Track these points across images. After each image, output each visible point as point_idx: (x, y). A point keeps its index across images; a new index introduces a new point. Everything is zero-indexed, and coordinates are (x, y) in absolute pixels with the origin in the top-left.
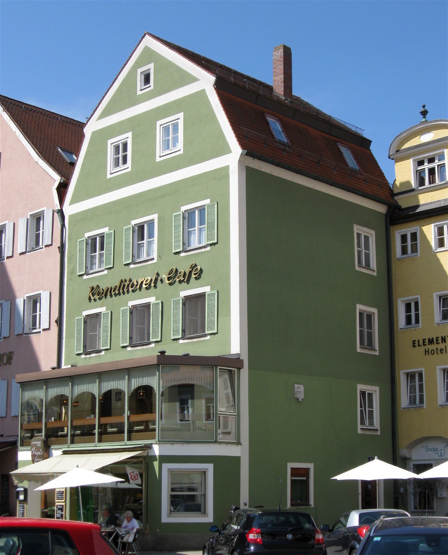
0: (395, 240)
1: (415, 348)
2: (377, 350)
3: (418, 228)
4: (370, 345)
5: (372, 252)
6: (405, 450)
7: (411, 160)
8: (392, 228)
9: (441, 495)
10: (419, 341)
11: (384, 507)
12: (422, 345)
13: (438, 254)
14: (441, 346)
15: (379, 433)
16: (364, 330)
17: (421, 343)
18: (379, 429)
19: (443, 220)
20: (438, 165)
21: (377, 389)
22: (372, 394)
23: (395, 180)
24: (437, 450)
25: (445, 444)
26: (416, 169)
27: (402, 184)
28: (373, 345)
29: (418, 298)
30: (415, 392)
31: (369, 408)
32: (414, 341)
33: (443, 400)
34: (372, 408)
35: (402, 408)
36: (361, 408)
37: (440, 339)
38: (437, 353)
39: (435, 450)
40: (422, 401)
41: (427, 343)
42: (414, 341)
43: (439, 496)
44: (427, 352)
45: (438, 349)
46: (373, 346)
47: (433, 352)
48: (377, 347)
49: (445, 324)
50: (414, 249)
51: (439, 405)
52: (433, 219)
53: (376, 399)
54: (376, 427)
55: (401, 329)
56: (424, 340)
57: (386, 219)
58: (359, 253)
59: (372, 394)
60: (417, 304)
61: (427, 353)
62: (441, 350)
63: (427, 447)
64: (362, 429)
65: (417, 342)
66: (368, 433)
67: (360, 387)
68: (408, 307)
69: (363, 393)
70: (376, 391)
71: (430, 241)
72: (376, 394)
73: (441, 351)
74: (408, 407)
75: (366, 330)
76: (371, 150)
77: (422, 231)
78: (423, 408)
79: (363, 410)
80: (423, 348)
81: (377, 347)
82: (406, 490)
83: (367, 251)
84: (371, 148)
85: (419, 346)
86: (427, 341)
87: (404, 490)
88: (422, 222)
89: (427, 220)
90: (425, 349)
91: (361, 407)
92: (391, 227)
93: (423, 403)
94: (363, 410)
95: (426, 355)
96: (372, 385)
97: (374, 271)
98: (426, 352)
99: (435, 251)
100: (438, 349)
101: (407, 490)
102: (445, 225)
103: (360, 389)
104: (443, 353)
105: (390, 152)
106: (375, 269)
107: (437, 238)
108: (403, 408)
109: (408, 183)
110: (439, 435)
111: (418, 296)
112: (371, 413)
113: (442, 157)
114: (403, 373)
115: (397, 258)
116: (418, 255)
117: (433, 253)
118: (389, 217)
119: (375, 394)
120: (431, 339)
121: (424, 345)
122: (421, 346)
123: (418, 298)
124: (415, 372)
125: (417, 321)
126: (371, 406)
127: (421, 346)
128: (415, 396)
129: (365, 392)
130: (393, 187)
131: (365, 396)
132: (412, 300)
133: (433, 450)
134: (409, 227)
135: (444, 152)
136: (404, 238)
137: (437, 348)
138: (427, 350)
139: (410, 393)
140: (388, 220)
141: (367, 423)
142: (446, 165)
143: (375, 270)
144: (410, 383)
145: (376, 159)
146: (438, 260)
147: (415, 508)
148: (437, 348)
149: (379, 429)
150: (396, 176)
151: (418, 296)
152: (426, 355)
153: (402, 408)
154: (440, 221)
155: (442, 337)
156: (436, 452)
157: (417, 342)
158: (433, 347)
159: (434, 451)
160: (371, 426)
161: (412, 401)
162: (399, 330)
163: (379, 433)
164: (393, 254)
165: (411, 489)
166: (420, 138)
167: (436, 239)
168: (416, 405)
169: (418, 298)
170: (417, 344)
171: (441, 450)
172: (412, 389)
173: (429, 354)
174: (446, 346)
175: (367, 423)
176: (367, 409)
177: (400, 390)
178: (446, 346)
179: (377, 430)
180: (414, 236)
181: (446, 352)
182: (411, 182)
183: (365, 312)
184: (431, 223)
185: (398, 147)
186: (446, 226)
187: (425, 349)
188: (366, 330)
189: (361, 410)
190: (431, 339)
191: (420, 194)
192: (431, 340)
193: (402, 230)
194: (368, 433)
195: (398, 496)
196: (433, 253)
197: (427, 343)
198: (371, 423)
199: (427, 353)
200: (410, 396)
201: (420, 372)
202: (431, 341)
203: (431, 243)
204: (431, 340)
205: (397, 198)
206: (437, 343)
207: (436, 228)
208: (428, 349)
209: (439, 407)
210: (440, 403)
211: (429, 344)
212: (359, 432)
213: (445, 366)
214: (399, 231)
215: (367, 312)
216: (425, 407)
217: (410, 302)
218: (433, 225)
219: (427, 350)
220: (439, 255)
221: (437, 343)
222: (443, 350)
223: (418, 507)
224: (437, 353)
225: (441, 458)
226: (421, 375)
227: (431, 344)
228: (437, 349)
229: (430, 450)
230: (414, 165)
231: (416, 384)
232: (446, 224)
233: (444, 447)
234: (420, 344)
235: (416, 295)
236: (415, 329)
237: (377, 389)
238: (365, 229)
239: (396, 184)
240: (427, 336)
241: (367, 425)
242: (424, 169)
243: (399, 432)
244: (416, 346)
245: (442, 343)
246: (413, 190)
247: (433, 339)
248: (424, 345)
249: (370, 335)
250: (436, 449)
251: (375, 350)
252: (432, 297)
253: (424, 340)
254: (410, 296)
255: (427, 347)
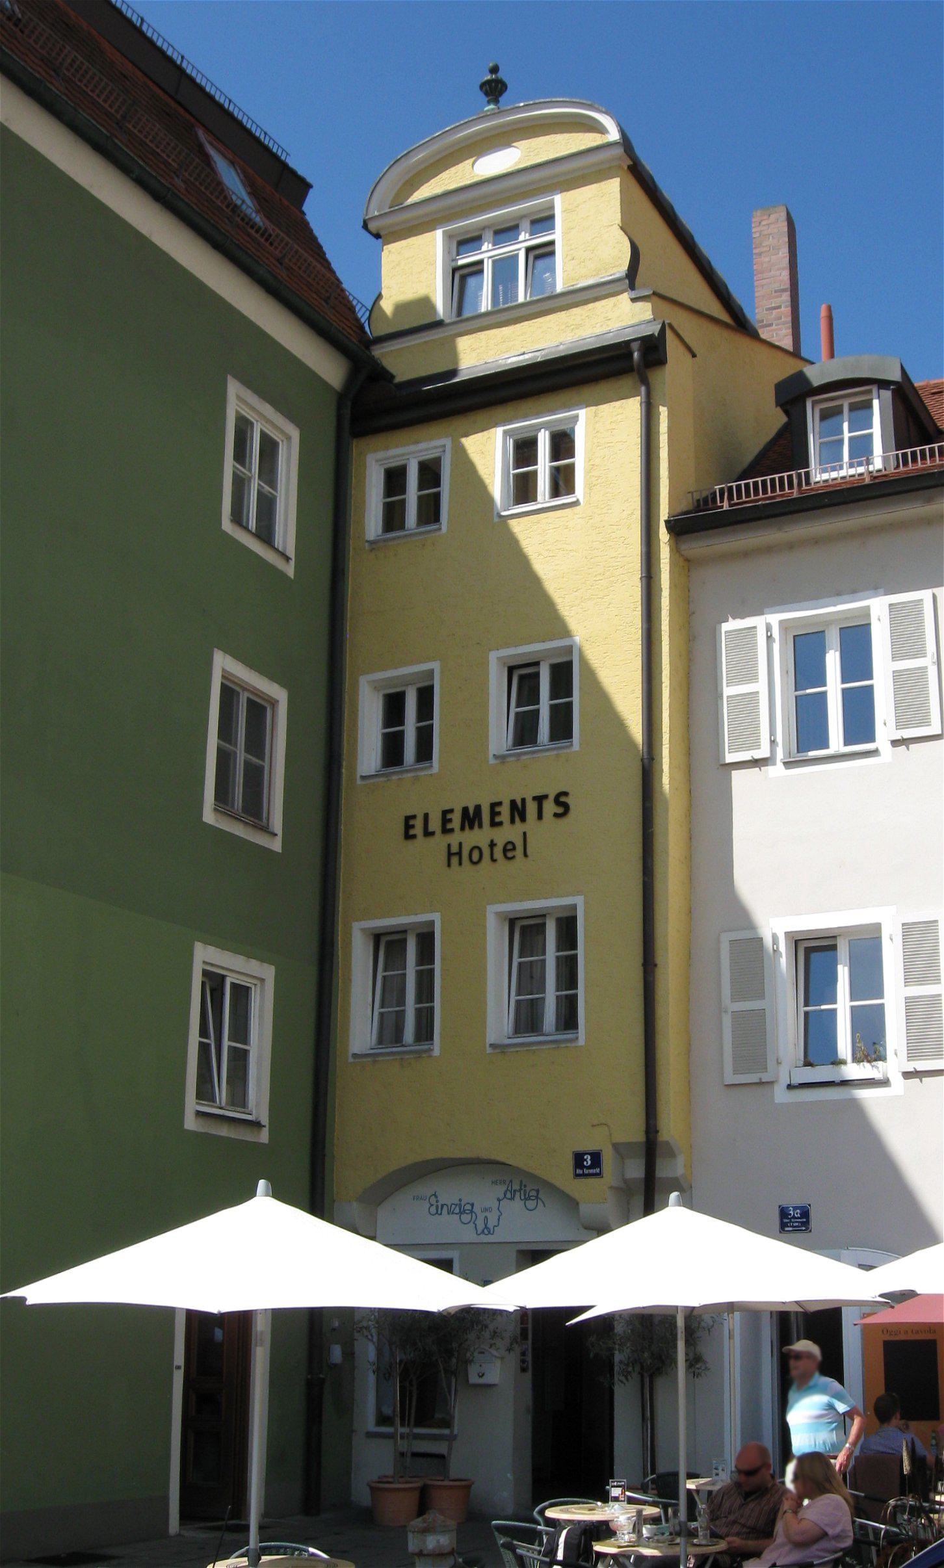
0: (365, 482)
1: (409, 843)
2: (276, 835)
3: (447, 442)
4: (254, 811)
5: (283, 492)
6: (355, 1204)
7: (439, 234)
8: (357, 447)
9: (481, 1376)
10: (426, 816)
11: (175, 1311)
12: (438, 831)
13: (513, 523)
14: (509, 832)
15: (264, 1137)
16: (235, 753)
17: (435, 824)
18: (265, 1121)
19: (538, 415)
20: (529, 250)
21: (268, 972)
22: (248, 989)
23: (379, 297)
24: (472, 1211)
25: (500, 1190)
26: (454, 264)
27: (401, 308)
28: (265, 815)
29: (431, 673)
30: (401, 1001)
31: (234, 1041)
32: (408, 819)
33: (506, 1028)
34: (245, 1041)
35: (350, 1055)
36: (201, 1036)
37: (505, 810)
38: (493, 860)
39: (463, 1210)
40: (425, 1031)
41: (456, 823)
42: (408, 819)
43: (474, 1379)
44: (453, 855)
45: (495, 845)
46: (265, 820)
47: (476, 856)
48: (277, 822)
49: (525, 757)
50: (430, 511)
51: (491, 1045)
52: (499, 412)
53: (261, 1010)
54: (254, 1112)
55: (363, 778)
56: (445, 813)
57: (340, 407)
58: (240, 484)
59: (248, 989)
60: (426, 696)
61: (455, 860)
62: (509, 848)
63: (433, 1200)
64: (199, 1114)
65: (419, 823)
66: (224, 1131)
67: (205, 955)
68: (394, 707)
69: (214, 982)
70: (262, 980)
71: (487, 481)
72: (289, 448)
73: (505, 850)
74: (372, 1051)
75: (241, 756)
76: (305, 211)
77: (461, 454)
78: (431, 1056)
79: (209, 1045)
80: (439, 842)
81: (277, 822)
82: (349, 1354)
83: (257, 761)
84: (305, 208)
85: (428, 833)
86: (456, 818)
87: (343, 1353)
88: (460, 422)
89: (480, 417)
90: (449, 846)
91: (204, 1032)
92: (355, 440)
93: (432, 1039)
94: (209, 1045)
95: (449, 865)
96: (249, 956)
97: (288, 559)
98: (450, 855)
99: (504, 513)
100: (495, 845)
101: (353, 1354)
102: (543, 430)
103: (204, 962)
104: (513, 857)
105: (372, 205)
106: (291, 553)
107: (512, 472)
108: (355, 1056)
109: (425, 303)
110: (485, 1155)
111: (435, 666)
112: (240, 1059)
113: (544, 221)
114: (363, 930)
115: (367, 541)
116: (440, 529)
117: (496, 520)
118: (349, 404)
119: (258, 992)
120: (471, 811)
121: (446, 831)
122: (433, 834)
123: (433, 670)
124: (403, 931)
125: (425, 751)
126: (241, 1031)
127: (433, 834)
128: (400, 1016)
129: (223, 977)
130: (369, 318)
131: (223, 994)
132: (407, 680)
133: (457, 1210)
134: (417, 442)
135: (552, 201)
136: (395, 479)
137: (492, 841)
138: (455, 849)
139: (382, 1006)
140: (347, 412)
141: (222, 1093)
142: (558, 248)
143: (289, 556)
144: (385, 970)
145: (321, 241)
146: (513, 543)
147: (383, 1420)
148: (492, 841)
149: (265, 1121)
150: (383, 286)
151: (435, 666)
152: (449, 865)
153: (350, 1055)
154: (525, 417)
155: (513, 803)
156: (466, 1218)
157: (419, 823)
158: (480, 837)
159: (461, 1213)
160: (239, 1109)
161: (390, 1031)
162: (359, 782)
163: (264, 1137)
164: (352, 530)
165: (368, 1351)
166: (473, 166)
167: (509, 476)
168: (403, 1046)
169: (433, 670)
170: (418, 830)
171: (486, 1210)
172: (392, 992)
173: (460, 864)
174: (525, 834)
175: (222, 1093)
176: (226, 1043)
177: (347, 993)
178: (525, 834)
179: (257, 1125)
180: (430, 473)
181: (526, 855)
182: (433, 299)
183: (245, 689)
184: (496, 425)
185: (397, 196)
186: (547, 432)
187: (449, 846)
188: (241, 756)
189: (201, 1043)
190: (471, 811)
191: (461, 335)
192: (471, 816)
193: (394, 452)
194: (224, 1131)
195: (321, 1376)
196: (496, 520)
197: (456, 823)
198: (239, 1097)
199: (455, 860)
200: (382, 1015)
201: (425, 930)
202: (471, 818)
203: (490, 488)
204: (471, 816)
205: (382, 351)
206: (494, 824)
207: (511, 444)
208: (460, 844)
209: (489, 1050)
210: (492, 1036)
211: (462, 828)
212: (191, 1123)
213: (439, 1031)
214: (381, 454)
215: (252, 693)
216: (436, 1052)
217: (398, 690)
218: (499, 431)
219: (455, 849)
220: (516, 526)
221: (494, 824)
222: (514, 848)
223: (398, 1421)
224: (493, 860)
225: (484, 1239)
226: (426, 940)
227: (471, 827)
228: (492, 845)
229: (445, 1208)
230: (447, 251)
231: (405, 975)
232: (546, 429)
233: (499, 1200)
234: (431, 829)
235: (429, 659)
236: (417, 778)
237: (268, 972)
238: (267, 409)
239: (381, 309)
240: (458, 802)
241: (223, 1104)
242: (481, 262)
243: (336, 1141)
244: (414, 837)
245: (513, 821)
246: (439, 324)
247: (478, 808)
248: (446, 831)
249: (255, 779)
250: (468, 1207)
251: (266, 830)
252: (485, 664)
253: (445, 813)
254: (403, 664)
255: (454, 839)
